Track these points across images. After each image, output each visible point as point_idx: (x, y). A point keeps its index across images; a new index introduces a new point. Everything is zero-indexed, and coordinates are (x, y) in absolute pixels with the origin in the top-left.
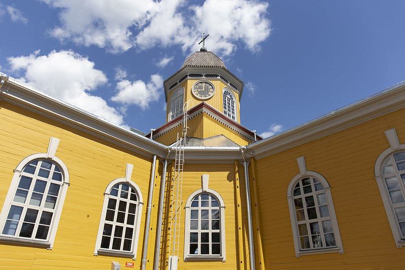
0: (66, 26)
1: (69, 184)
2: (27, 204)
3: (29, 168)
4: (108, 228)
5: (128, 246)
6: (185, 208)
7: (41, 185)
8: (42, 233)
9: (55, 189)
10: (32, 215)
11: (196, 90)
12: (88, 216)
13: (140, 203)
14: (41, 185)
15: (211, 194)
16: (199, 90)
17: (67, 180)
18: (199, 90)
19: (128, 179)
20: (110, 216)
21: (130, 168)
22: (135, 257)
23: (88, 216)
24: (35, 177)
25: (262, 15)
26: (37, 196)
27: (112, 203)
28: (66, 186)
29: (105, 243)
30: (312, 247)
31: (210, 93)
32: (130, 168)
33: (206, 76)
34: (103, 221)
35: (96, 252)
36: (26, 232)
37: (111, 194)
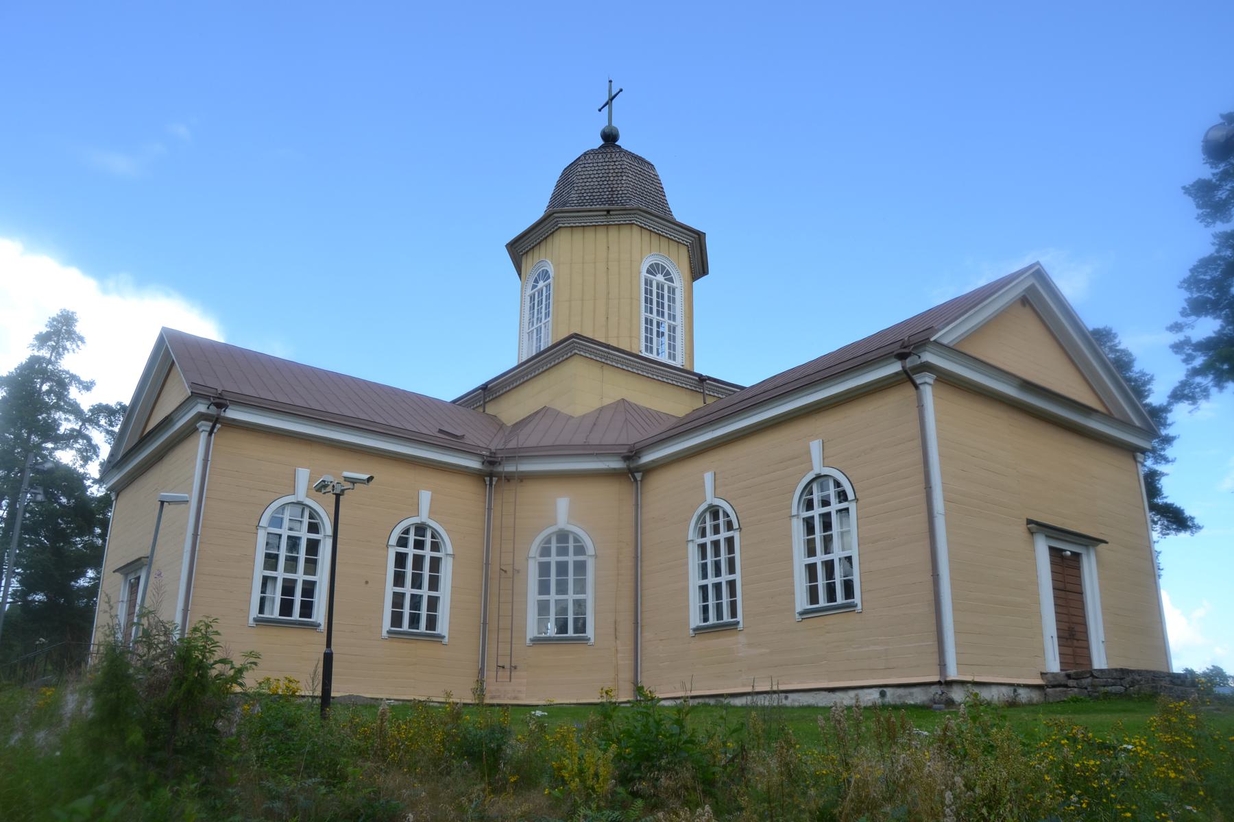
0: (1168, 534)
4: (398, 600)
12: (367, 582)
13: (447, 555)
15: (575, 533)
19: (424, 517)
20: (399, 579)
21: (425, 497)
23: (367, 582)
25: (1147, 397)
26: (718, 573)
27: (401, 559)
30: (571, 633)
32: (425, 497)
34: (390, 589)
35: (384, 634)
37: (542, 555)
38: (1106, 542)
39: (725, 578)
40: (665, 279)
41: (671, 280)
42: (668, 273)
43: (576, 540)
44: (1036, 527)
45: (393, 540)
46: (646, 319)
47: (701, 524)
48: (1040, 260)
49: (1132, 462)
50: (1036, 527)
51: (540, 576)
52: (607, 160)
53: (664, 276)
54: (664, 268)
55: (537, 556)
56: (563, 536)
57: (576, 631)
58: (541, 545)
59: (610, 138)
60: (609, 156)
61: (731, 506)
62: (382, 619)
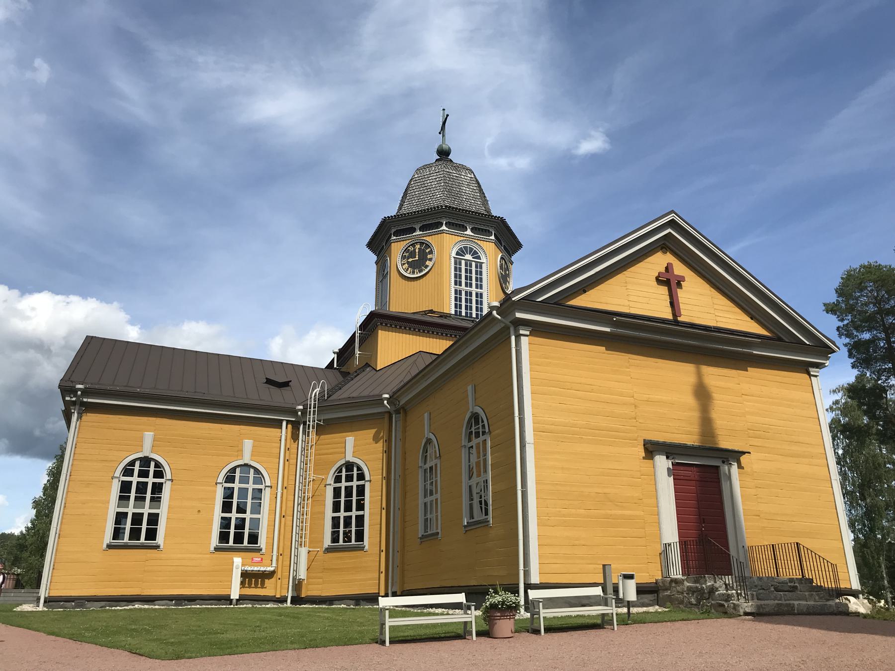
1: (172, 480)
2: (131, 509)
3: (128, 472)
4: (361, 507)
5: (360, 536)
6: (325, 486)
7: (142, 488)
8: (152, 534)
9: (158, 488)
10: (137, 519)
11: (405, 261)
12: (199, 511)
13: (266, 486)
14: (142, 488)
16: (410, 260)
17: (169, 476)
18: (410, 260)
21: (248, 444)
22: (264, 551)
23: (199, 511)
24: (135, 479)
26: (140, 499)
28: (169, 483)
29: (224, 537)
31: (428, 263)
33: (421, 229)
36: (135, 534)
38: (750, 453)
39: (354, 513)
40: (473, 258)
41: (479, 258)
42: (475, 253)
43: (359, 469)
44: (652, 449)
45: (221, 479)
46: (456, 291)
47: (337, 473)
48: (691, 218)
49: (807, 376)
50: (652, 449)
51: (334, 498)
52: (432, 172)
53: (472, 256)
54: (471, 249)
55: (332, 482)
56: (349, 466)
57: (344, 541)
58: (336, 474)
59: (444, 154)
60: (433, 169)
61: (723, 388)
62: (210, 538)
